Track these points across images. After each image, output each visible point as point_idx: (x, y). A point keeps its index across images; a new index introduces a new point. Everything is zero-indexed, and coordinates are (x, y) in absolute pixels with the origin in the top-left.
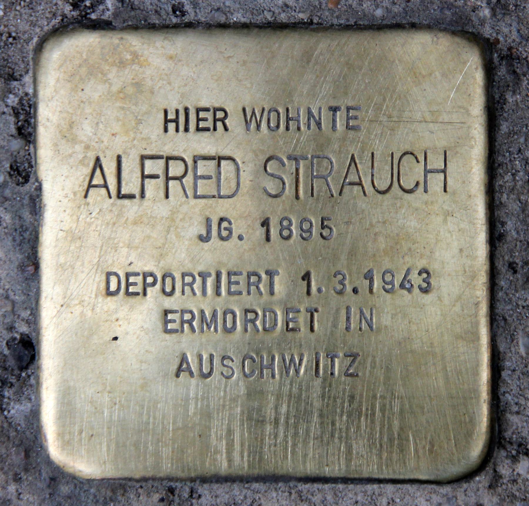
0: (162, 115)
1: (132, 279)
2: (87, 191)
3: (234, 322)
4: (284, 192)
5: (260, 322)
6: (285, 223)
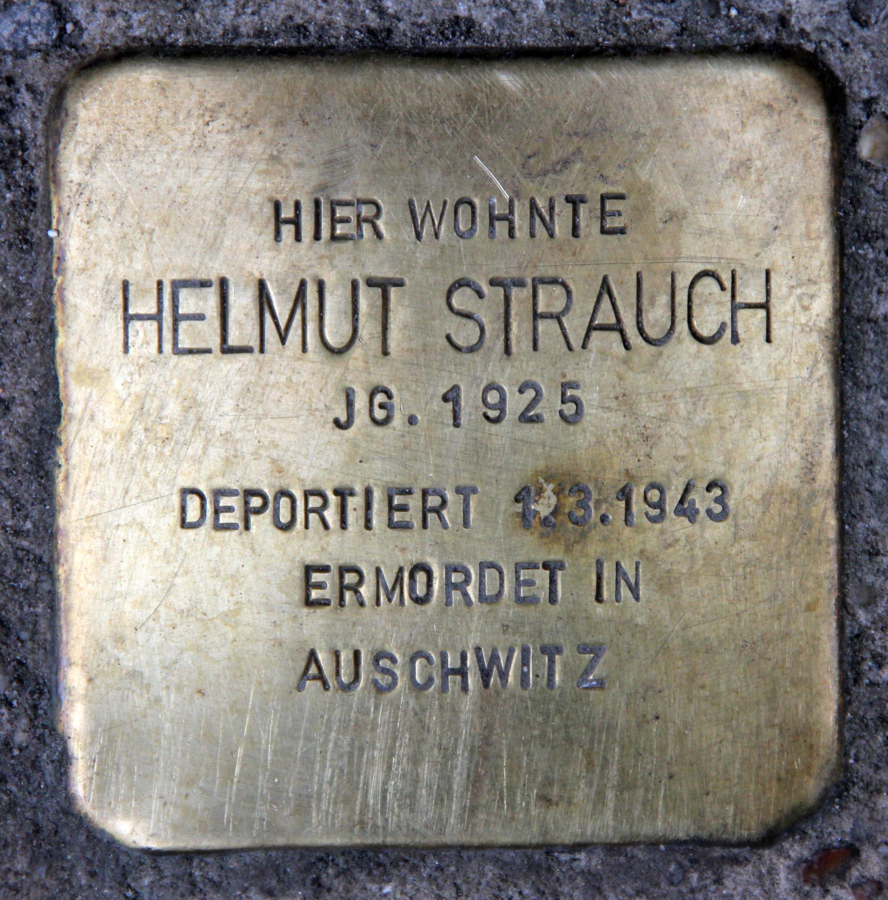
0: (269, 210)
1: (224, 502)
2: (587, 336)
3: (429, 585)
4: (482, 344)
5: (475, 587)
6: (493, 397)
